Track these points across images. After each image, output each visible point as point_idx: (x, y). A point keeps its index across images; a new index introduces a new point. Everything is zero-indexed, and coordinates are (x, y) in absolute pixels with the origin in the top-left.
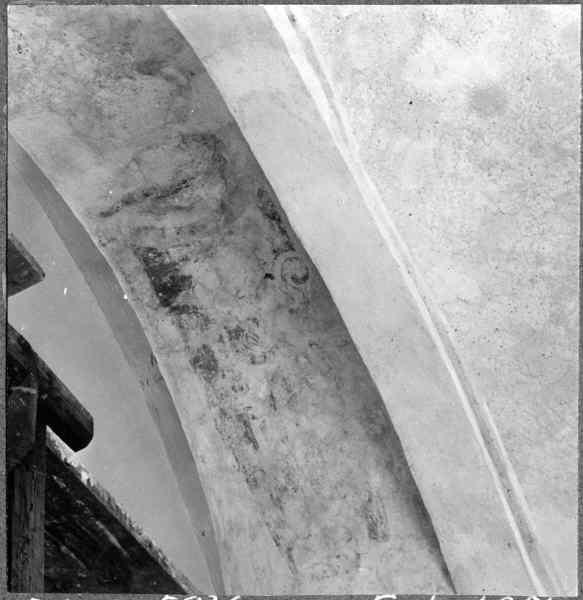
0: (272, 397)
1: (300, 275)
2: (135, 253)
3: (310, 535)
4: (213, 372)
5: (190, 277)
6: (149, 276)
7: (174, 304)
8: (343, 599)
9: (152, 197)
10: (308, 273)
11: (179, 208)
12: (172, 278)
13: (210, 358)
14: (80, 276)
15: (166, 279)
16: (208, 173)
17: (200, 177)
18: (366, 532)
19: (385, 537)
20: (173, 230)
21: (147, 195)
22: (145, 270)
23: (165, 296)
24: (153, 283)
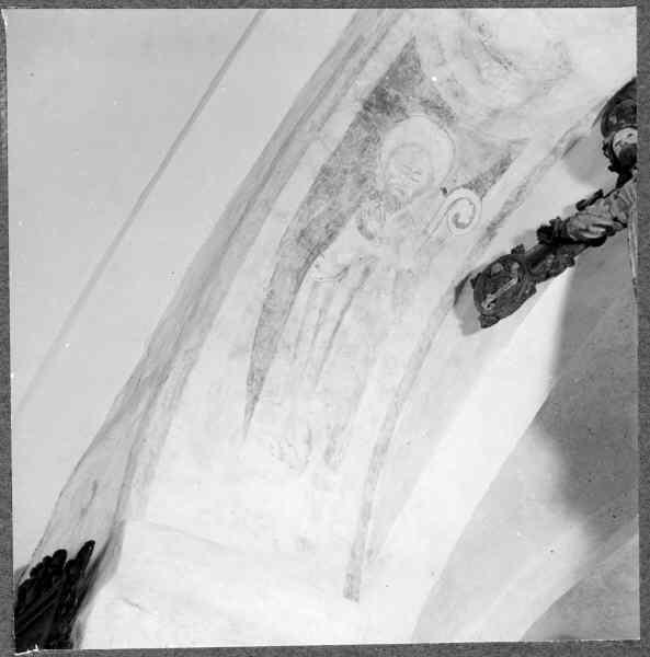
0: (346, 269)
1: (460, 220)
2: (407, 45)
3: (279, 404)
4: (327, 196)
5: (407, 117)
6: (388, 73)
7: (370, 115)
8: (4, 222)
9: (480, 36)
10: (468, 225)
11: (479, 70)
12: (397, 98)
13: (338, 185)
14: (636, 305)
15: (392, 92)
16: (529, 83)
17: (521, 77)
18: (324, 448)
19: (334, 468)
20: (449, 74)
21: (480, 30)
22: (392, 66)
23: (374, 102)
24: (382, 81)
